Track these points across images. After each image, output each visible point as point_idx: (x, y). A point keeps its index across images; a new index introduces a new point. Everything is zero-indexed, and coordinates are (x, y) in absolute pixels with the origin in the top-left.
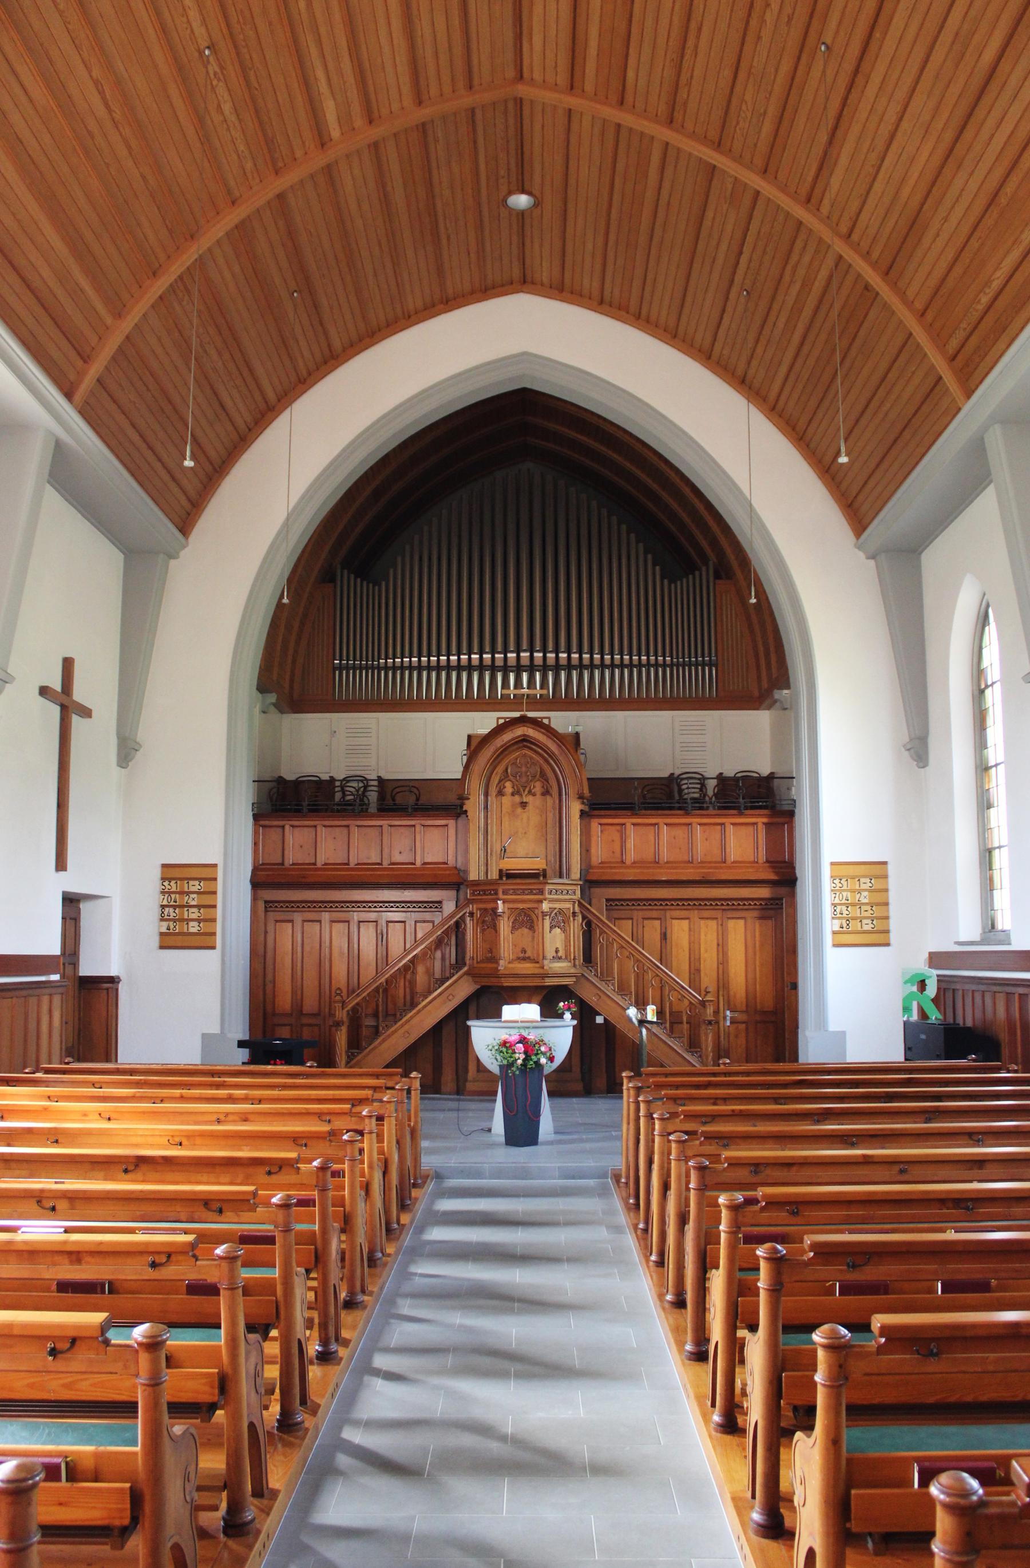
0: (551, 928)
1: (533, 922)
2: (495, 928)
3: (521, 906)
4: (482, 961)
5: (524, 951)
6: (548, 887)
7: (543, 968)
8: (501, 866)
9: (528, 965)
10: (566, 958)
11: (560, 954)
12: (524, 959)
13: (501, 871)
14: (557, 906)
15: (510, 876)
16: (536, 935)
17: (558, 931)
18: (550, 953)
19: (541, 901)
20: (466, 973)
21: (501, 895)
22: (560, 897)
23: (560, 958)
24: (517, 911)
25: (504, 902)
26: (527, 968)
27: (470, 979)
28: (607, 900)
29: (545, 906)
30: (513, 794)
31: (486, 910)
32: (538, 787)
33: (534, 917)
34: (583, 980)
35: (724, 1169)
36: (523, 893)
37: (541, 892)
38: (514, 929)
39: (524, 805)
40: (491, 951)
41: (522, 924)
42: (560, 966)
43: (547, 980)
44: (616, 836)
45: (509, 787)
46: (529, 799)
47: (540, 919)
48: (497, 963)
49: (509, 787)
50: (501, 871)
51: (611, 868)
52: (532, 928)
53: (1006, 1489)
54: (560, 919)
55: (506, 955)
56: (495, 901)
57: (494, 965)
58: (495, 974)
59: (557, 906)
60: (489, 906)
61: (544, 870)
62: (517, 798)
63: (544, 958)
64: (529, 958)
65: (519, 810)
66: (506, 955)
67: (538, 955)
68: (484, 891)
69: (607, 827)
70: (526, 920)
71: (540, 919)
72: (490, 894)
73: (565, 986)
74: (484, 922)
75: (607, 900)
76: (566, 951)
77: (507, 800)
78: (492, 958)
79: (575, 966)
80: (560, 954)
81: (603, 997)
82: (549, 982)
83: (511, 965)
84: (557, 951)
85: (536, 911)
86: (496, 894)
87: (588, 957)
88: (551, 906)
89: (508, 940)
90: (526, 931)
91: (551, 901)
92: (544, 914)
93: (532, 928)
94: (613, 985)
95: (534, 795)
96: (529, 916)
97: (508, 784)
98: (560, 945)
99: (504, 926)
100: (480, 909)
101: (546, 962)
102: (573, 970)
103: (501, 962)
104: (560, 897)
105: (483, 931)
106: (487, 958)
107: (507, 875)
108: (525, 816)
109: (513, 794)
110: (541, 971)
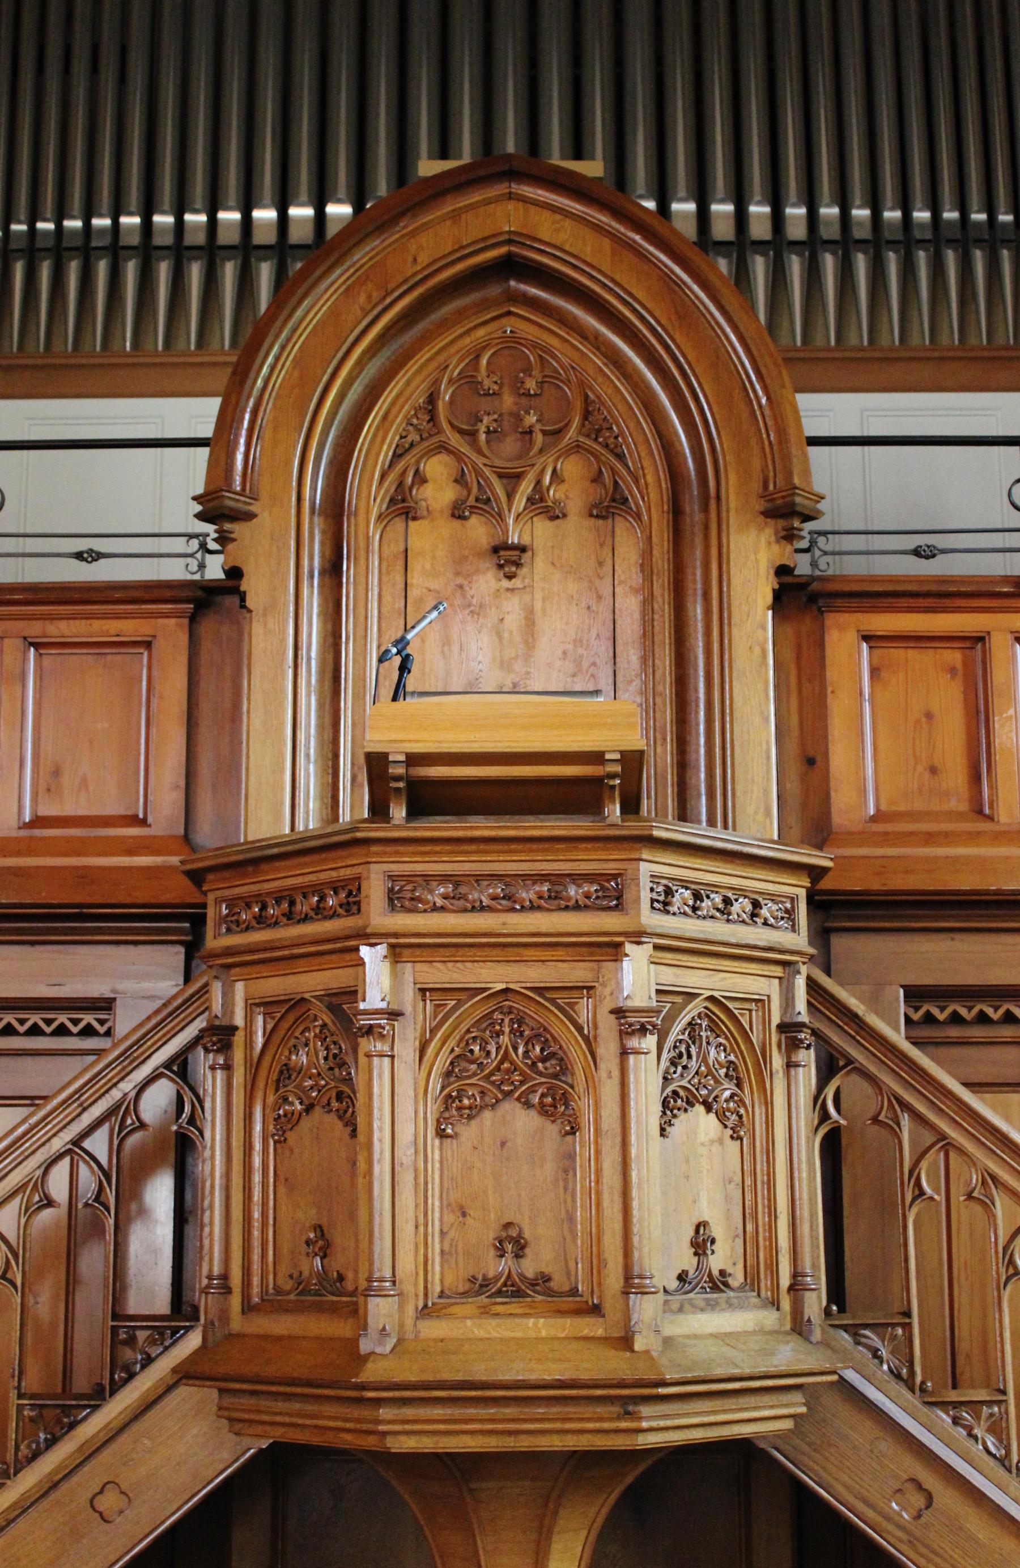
0: (671, 1106)
1: (564, 1068)
2: (344, 1103)
3: (495, 976)
4: (272, 1304)
5: (512, 1242)
6: (650, 868)
7: (626, 1342)
8: (376, 740)
9: (541, 1327)
10: (752, 1281)
11: (716, 1262)
12: (514, 1289)
13: (376, 764)
14: (704, 979)
15: (429, 797)
16: (582, 1146)
17: (701, 1125)
18: (663, 1256)
19: (611, 949)
20: (186, 1374)
21: (377, 915)
22: (718, 930)
23: (719, 1283)
24: (473, 1010)
25: (396, 953)
26: (528, 1345)
27: (211, 1394)
28: (915, 994)
29: (636, 977)
30: (458, 513)
31: (297, 1004)
32: (572, 483)
33: (576, 1053)
34: (843, 1412)
35: (220, 911)
36: (510, 903)
37: (613, 894)
38: (455, 1108)
39: (508, 557)
40: (322, 1242)
41: (504, 1086)
42: (725, 1334)
43: (650, 1415)
44: (947, 699)
45: (438, 490)
46: (539, 533)
47: (608, 1049)
48: (356, 1313)
49: (438, 490)
50: (376, 764)
51: (930, 838)
52: (558, 1106)
53: (189, 867)
54: (714, 1060)
55: (407, 1263)
56: (345, 950)
57: (341, 1328)
58: (340, 1375)
59: (704, 979)
60: (312, 982)
61: (633, 762)
62: (478, 530)
63: (632, 1282)
64: (542, 1282)
65: (487, 582)
66: (407, 1263)
67: (596, 1264)
68: (287, 897)
69: (897, 654)
70: (522, 1058)
71: (608, 1049)
72: (320, 912)
73: (743, 1453)
74: (287, 1072)
75: (915, 994)
76: (749, 1241)
77: (430, 539)
78: (334, 1289)
79: (799, 1327)
80: (716, 1262)
81: (945, 1497)
82: (663, 1428)
83: (433, 1329)
84: (701, 1243)
85: (584, 1011)
86: (353, 905)
87: (849, 1286)
88: (669, 977)
89: (421, 1174)
90: (520, 1121)
91: (669, 948)
92: (630, 1023)
93: (558, 1106)
94: (997, 1429)
95: (555, 514)
96: (541, 1035)
97: (438, 468)
98: (715, 1205)
99: (398, 1092)
100: (268, 1005)
101: (646, 1310)
102: (788, 1355)
103: (381, 1310)
104: (718, 930)
105: (283, 1126)
106: (301, 1285)
107: (421, 791)
108: (513, 609)
109: (458, 513)
110: (613, 1365)
